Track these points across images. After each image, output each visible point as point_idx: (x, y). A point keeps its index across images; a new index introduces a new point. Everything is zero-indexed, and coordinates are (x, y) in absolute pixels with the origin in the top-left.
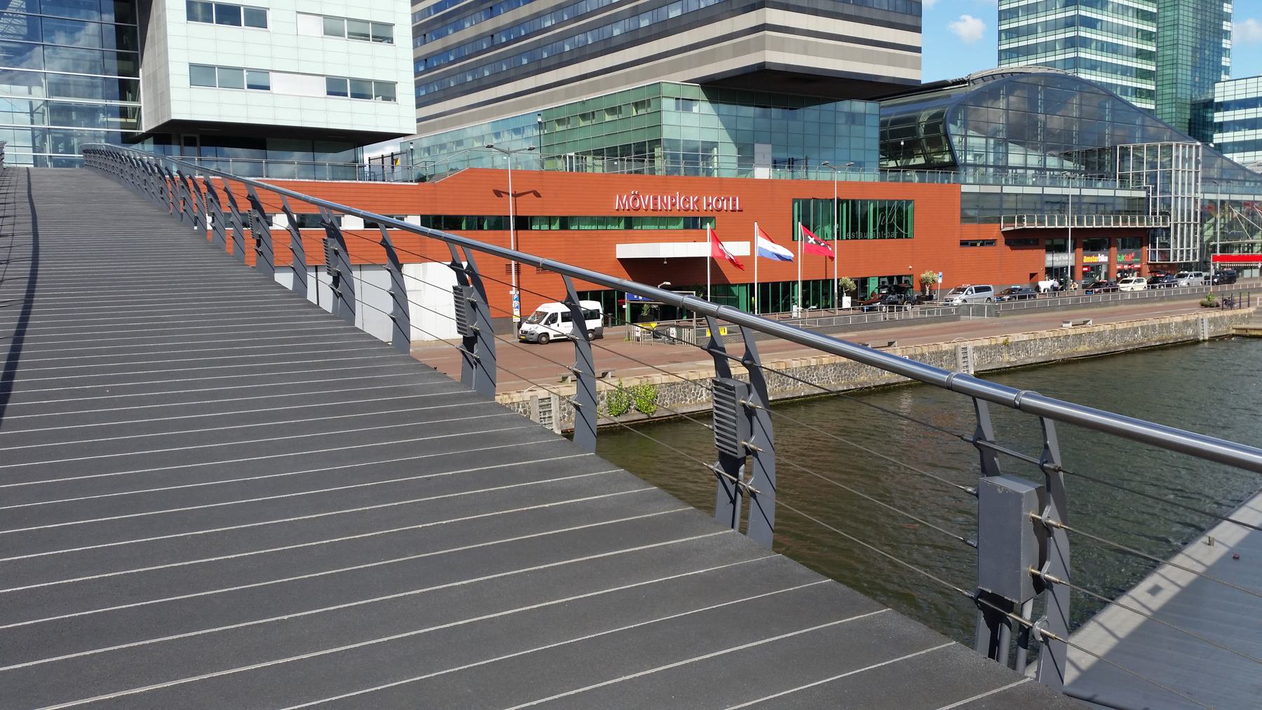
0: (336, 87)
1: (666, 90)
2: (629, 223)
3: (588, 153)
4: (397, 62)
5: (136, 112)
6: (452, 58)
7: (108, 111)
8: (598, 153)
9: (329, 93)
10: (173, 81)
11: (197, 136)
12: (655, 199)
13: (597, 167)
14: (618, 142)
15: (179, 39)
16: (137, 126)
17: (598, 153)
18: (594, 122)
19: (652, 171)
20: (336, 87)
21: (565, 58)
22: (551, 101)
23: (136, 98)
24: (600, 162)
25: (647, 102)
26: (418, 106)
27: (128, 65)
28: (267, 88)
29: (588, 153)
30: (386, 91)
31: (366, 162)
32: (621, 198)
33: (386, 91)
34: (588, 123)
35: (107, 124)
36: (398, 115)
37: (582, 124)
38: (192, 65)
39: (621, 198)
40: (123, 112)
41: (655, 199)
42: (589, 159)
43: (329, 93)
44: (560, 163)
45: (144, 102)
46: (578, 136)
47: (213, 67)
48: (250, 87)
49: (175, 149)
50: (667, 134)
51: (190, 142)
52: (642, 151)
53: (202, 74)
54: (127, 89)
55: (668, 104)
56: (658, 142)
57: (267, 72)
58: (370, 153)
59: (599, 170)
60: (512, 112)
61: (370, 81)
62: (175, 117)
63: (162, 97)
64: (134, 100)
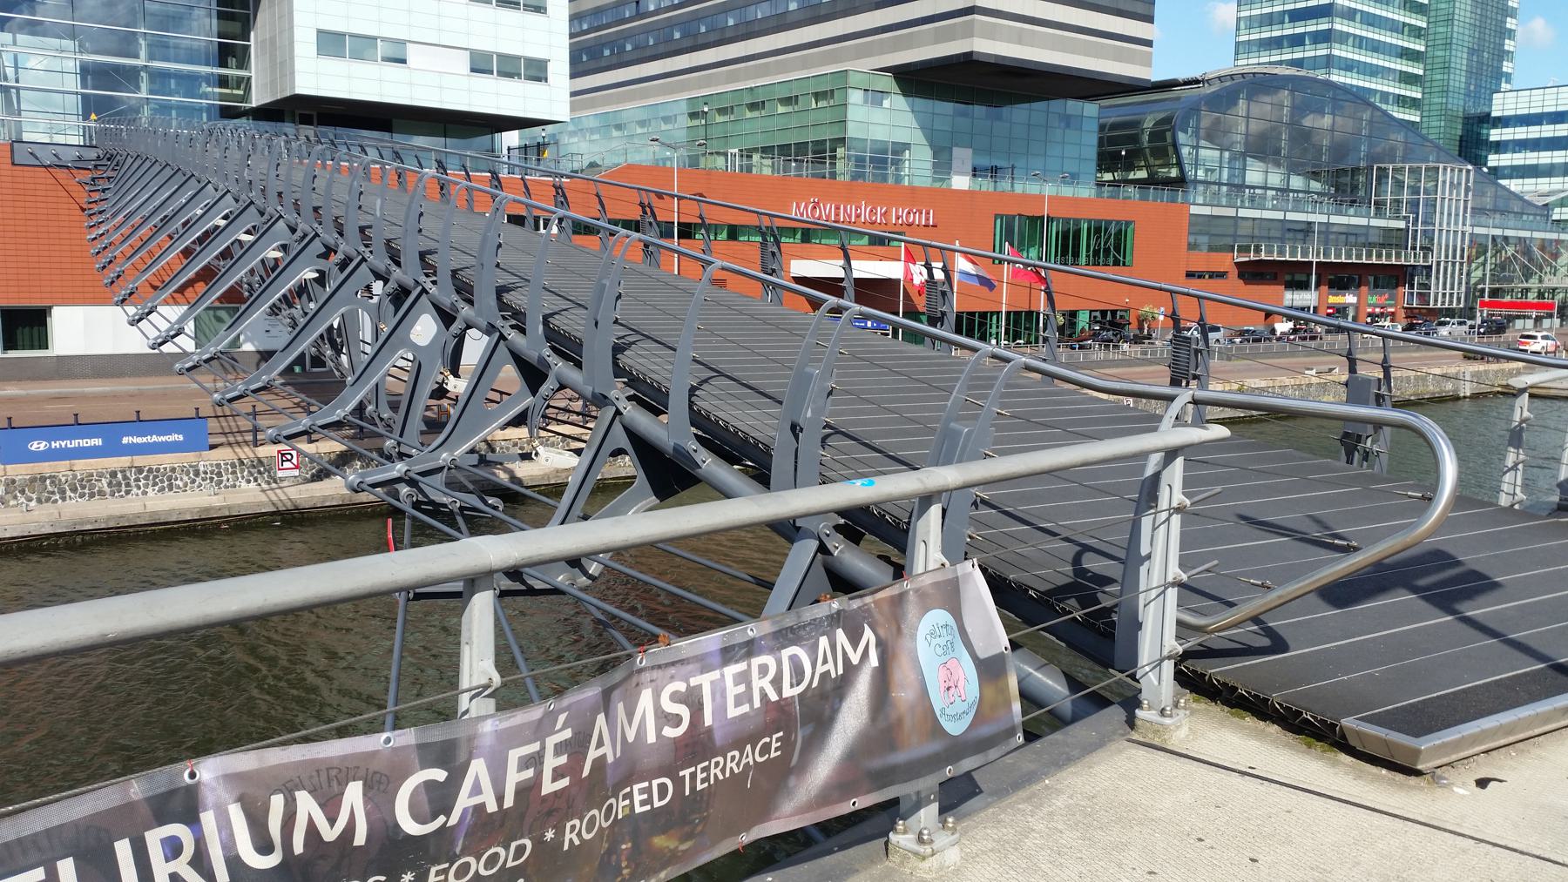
0: (481, 64)
1: (853, 79)
2: (807, 236)
3: (756, 150)
4: (548, 35)
5: (245, 83)
6: (585, 27)
7: (208, 79)
8: (766, 150)
9: (473, 70)
10: (299, 49)
12: (838, 208)
13: (764, 167)
14: (793, 139)
17: (766, 150)
18: (763, 113)
19: (833, 175)
20: (481, 64)
21: (728, 35)
22: (708, 86)
23: (243, 63)
24: (769, 162)
25: (830, 93)
26: (573, 76)
27: (235, 27)
28: (404, 61)
29: (756, 150)
30: (536, 71)
31: (505, 152)
32: (798, 207)
33: (536, 71)
34: (756, 114)
35: (206, 96)
36: (549, 99)
37: (749, 115)
38: (320, 32)
39: (798, 207)
40: (223, 82)
41: (838, 208)
42: (756, 157)
43: (473, 70)
44: (720, 161)
45: (255, 70)
46: (746, 128)
47: (344, 35)
50: (852, 131)
51: (306, 120)
52: (822, 153)
54: (230, 53)
55: (855, 97)
56: (842, 141)
57: (403, 43)
58: (511, 138)
59: (767, 171)
60: (678, 98)
61: (519, 58)
62: (299, 91)
63: (283, 64)
64: (240, 66)
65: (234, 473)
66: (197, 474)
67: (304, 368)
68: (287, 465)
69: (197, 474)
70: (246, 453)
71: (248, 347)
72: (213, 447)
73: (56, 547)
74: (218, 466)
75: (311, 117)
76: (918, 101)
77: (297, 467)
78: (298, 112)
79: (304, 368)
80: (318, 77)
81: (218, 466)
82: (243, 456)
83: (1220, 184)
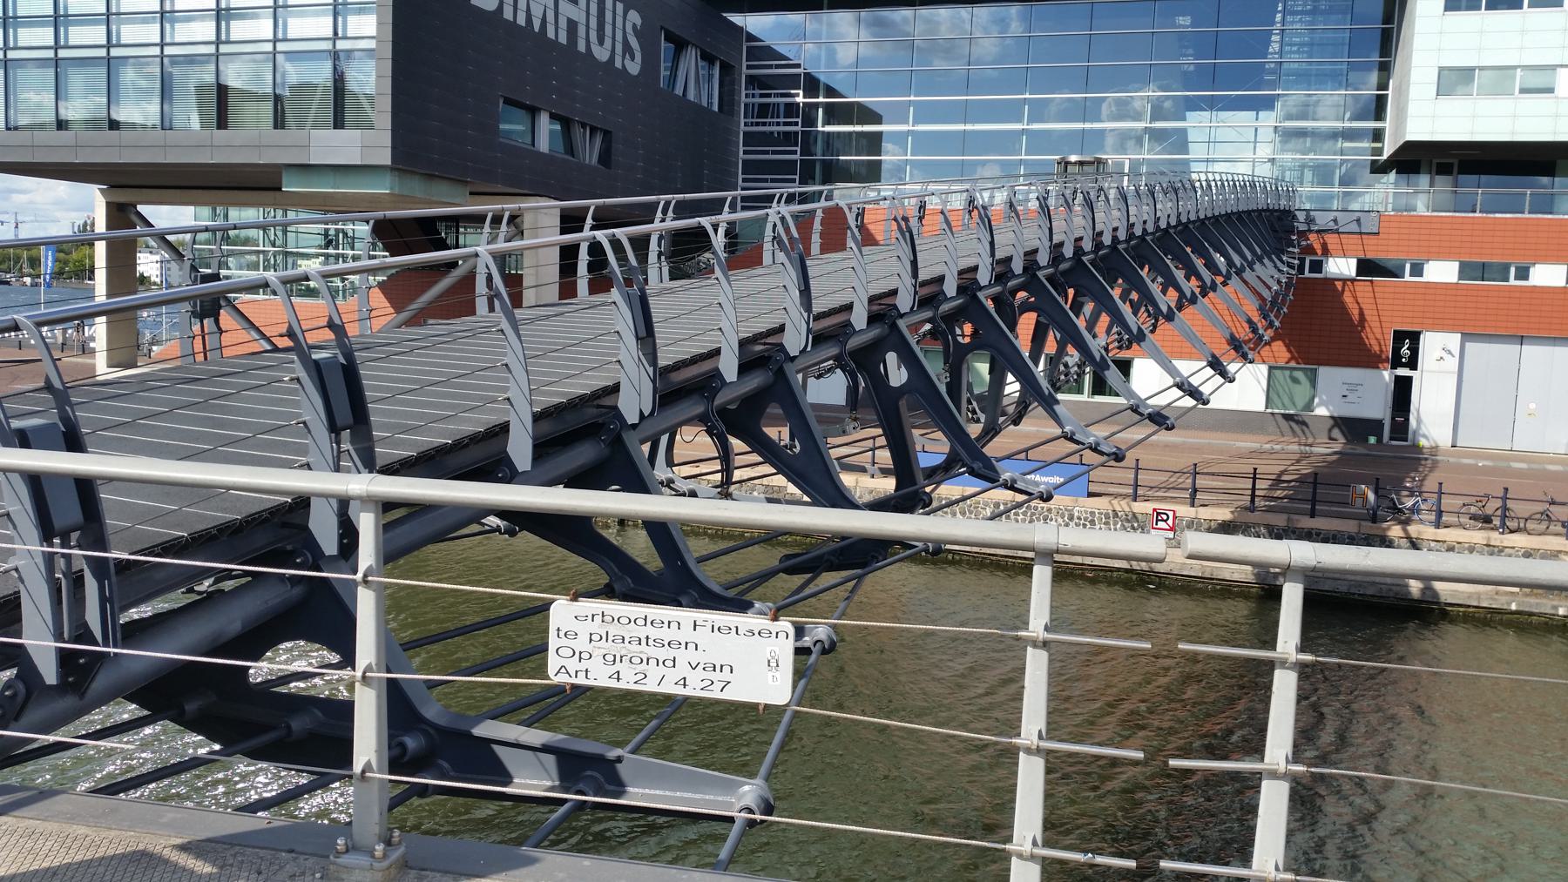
11: (1456, 162)
15: (1433, 35)
16: (1379, 152)
28: (1551, 90)
38: (1441, 69)
45: (1387, 125)
47: (1472, 69)
48: (1523, 91)
49: (1424, 180)
51: (1444, 170)
53: (1455, 80)
65: (1106, 523)
66: (1071, 518)
67: (1380, 440)
68: (1161, 525)
69: (1071, 518)
70: (1122, 506)
71: (1321, 411)
72: (1091, 495)
73: (959, 563)
74: (1092, 513)
75: (1451, 165)
76: (865, 13)
77: (1171, 529)
78: (1435, 161)
79: (1380, 440)
80: (1425, 116)
81: (1092, 513)
82: (1118, 508)
83: (162, 56)
